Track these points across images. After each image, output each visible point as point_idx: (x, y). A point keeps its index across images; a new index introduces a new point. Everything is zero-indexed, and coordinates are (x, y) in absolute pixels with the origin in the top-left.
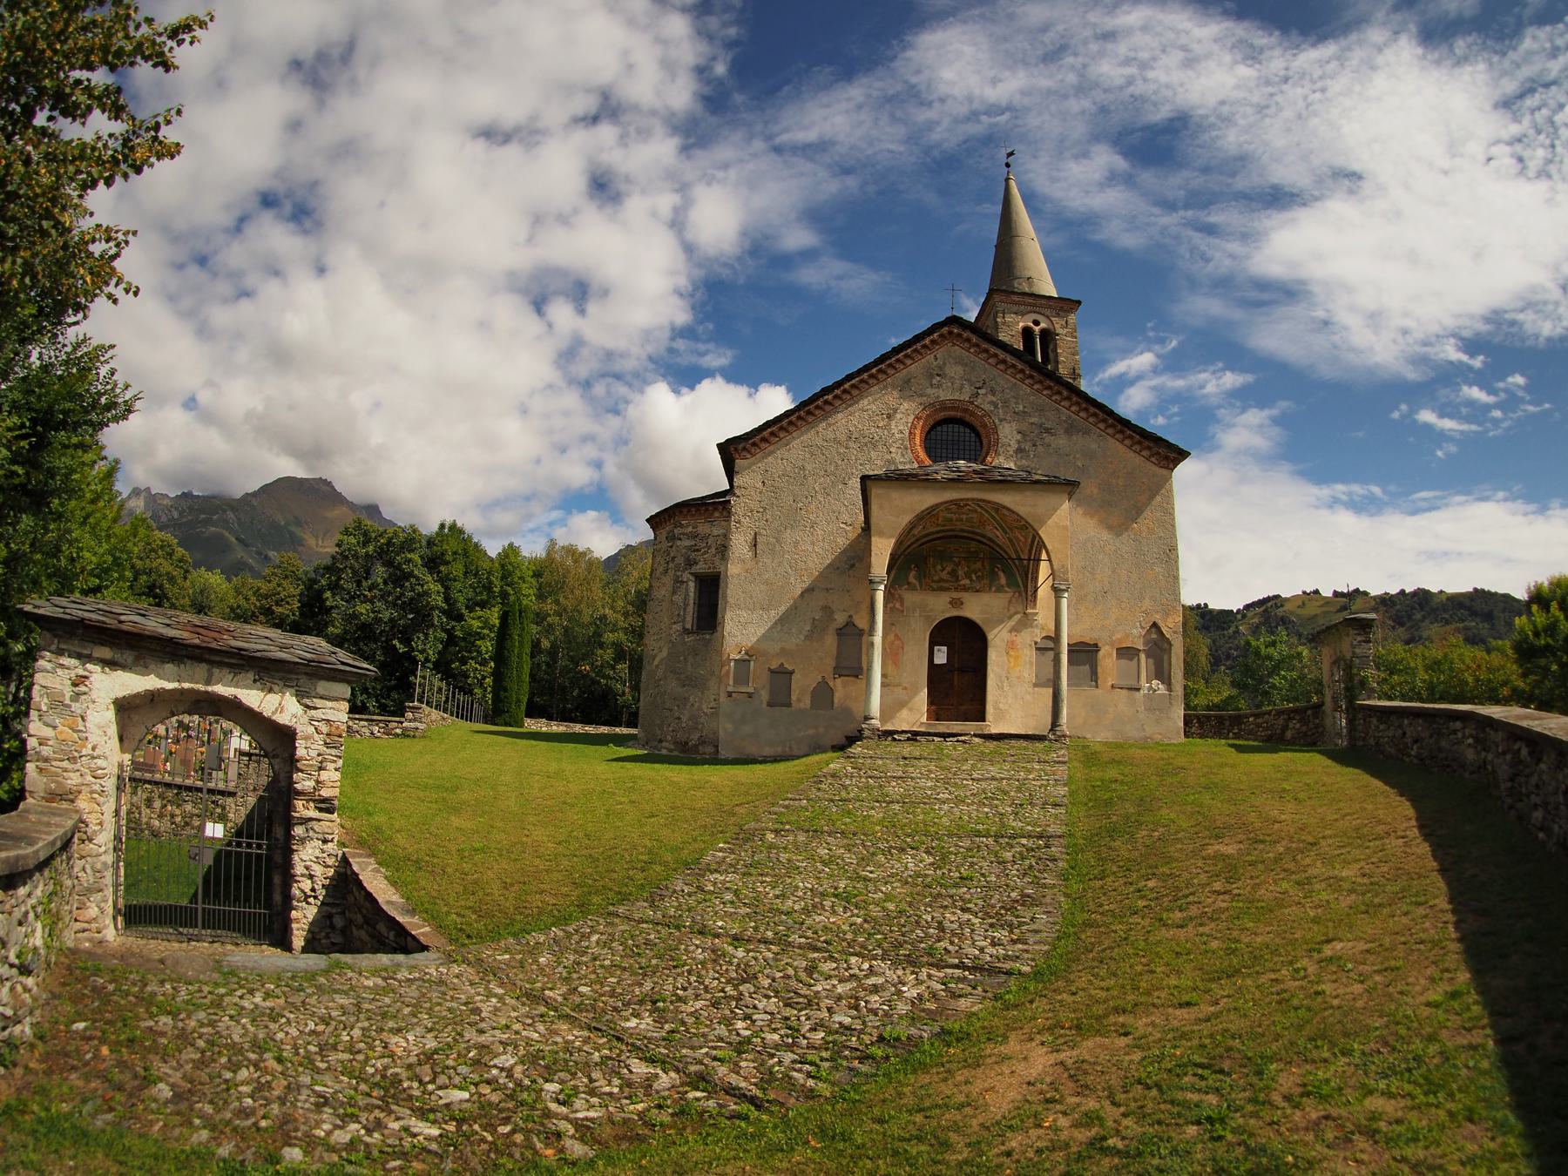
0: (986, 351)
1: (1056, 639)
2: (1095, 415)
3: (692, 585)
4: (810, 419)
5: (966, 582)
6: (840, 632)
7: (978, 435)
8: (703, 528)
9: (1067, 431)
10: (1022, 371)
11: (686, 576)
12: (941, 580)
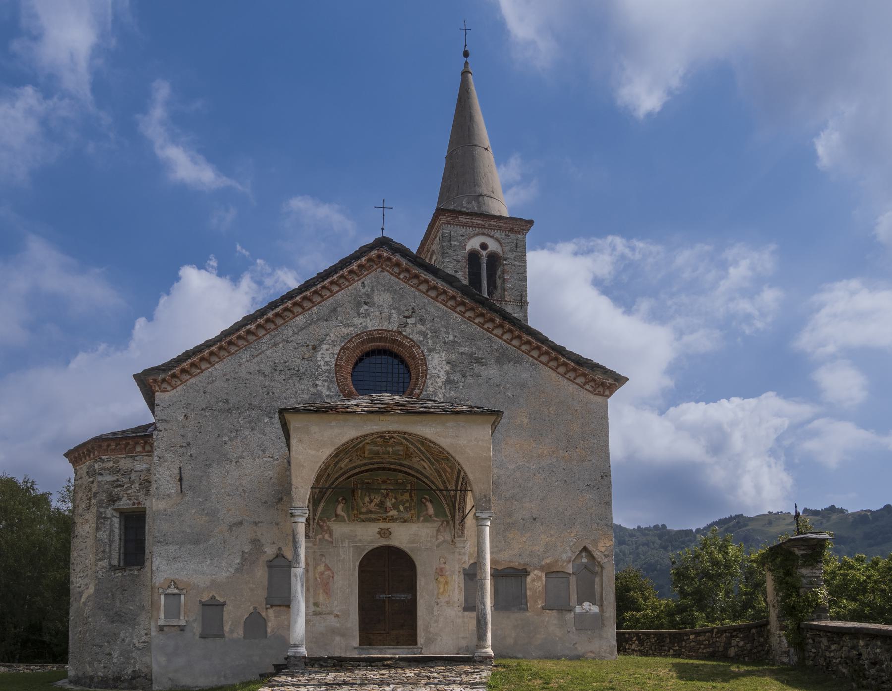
0: (416, 276)
1: (477, 564)
2: (528, 342)
3: (116, 521)
4: (233, 349)
5: (394, 513)
6: (270, 564)
7: (407, 367)
8: (125, 463)
9: (498, 361)
10: (454, 298)
11: (109, 512)
12: (371, 512)
